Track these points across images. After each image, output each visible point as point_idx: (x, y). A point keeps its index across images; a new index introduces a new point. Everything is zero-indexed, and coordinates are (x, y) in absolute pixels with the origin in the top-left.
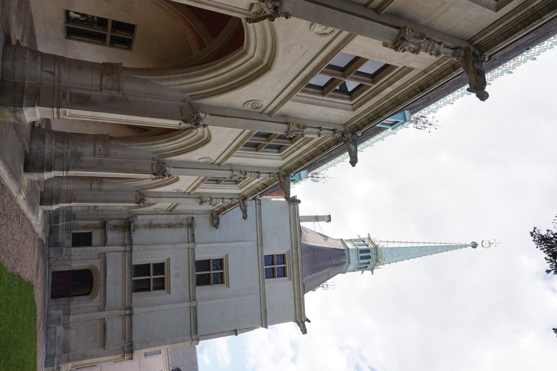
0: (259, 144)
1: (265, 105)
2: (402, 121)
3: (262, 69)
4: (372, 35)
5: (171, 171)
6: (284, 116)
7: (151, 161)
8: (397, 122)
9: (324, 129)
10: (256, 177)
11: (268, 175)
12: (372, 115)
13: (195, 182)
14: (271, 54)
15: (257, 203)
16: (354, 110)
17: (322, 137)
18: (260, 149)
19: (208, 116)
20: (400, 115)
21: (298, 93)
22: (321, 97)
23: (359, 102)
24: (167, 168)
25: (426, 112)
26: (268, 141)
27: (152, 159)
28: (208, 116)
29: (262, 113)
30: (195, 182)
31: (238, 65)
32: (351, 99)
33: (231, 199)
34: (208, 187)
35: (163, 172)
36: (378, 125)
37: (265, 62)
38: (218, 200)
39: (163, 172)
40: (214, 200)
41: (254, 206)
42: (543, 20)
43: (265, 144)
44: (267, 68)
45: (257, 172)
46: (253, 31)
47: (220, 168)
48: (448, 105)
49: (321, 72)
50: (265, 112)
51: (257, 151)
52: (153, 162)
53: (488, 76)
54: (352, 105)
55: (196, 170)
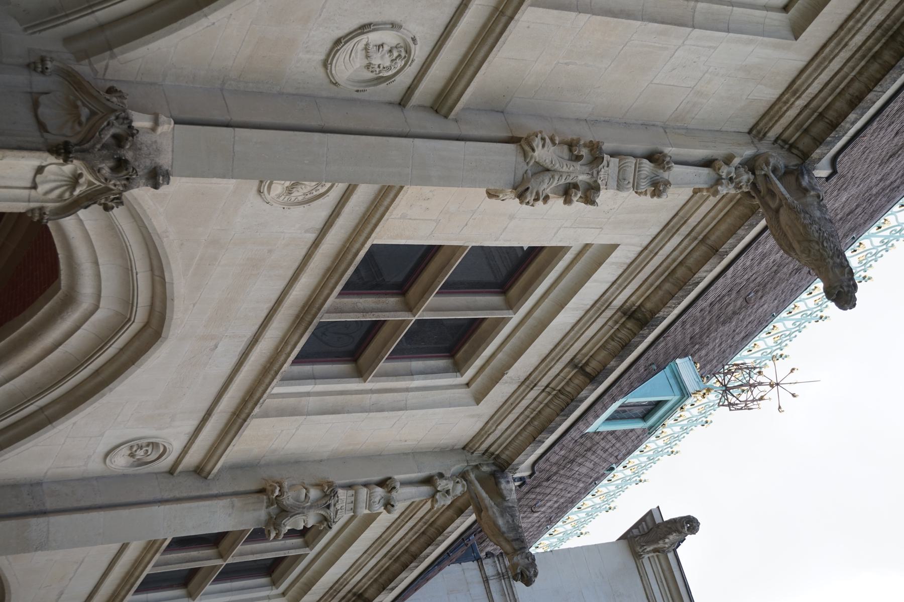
0: (194, 571)
1: (176, 447)
2: (673, 398)
3: (145, 331)
4: (448, 178)
5: (161, 138)
6: (496, 107)
7: (21, 79)
8: (658, 404)
9: (404, 483)
10: (378, 508)
11: (425, 489)
12: (387, 563)
13: (255, 340)
14: (153, 298)
15: (490, 570)
16: (478, 398)
17: (400, 507)
18: (201, 586)
19: (166, 126)
20: (661, 378)
21: (277, 389)
22: (354, 385)
23: (507, 348)
24: (141, 122)
25: (789, 324)
26: (410, 308)
27: (31, 67)
28: (166, 126)
29: (171, 471)
30: (255, 340)
31: (66, 336)
32: (274, 583)
33: (428, 481)
34: (312, 402)
35: (119, 140)
36: (598, 425)
37: (140, 316)
38: (364, 492)
39: (119, 140)
40: (341, 492)
41: (479, 589)
42: (438, 545)
43: (402, 323)
44: (153, 332)
45: (382, 484)
46: (83, 235)
47: (452, 128)
48: (812, 326)
49: (282, 380)
50: (180, 468)
51: (361, 374)
52: (40, 82)
53: (853, 259)
54: (468, 385)
55: (317, 136)
